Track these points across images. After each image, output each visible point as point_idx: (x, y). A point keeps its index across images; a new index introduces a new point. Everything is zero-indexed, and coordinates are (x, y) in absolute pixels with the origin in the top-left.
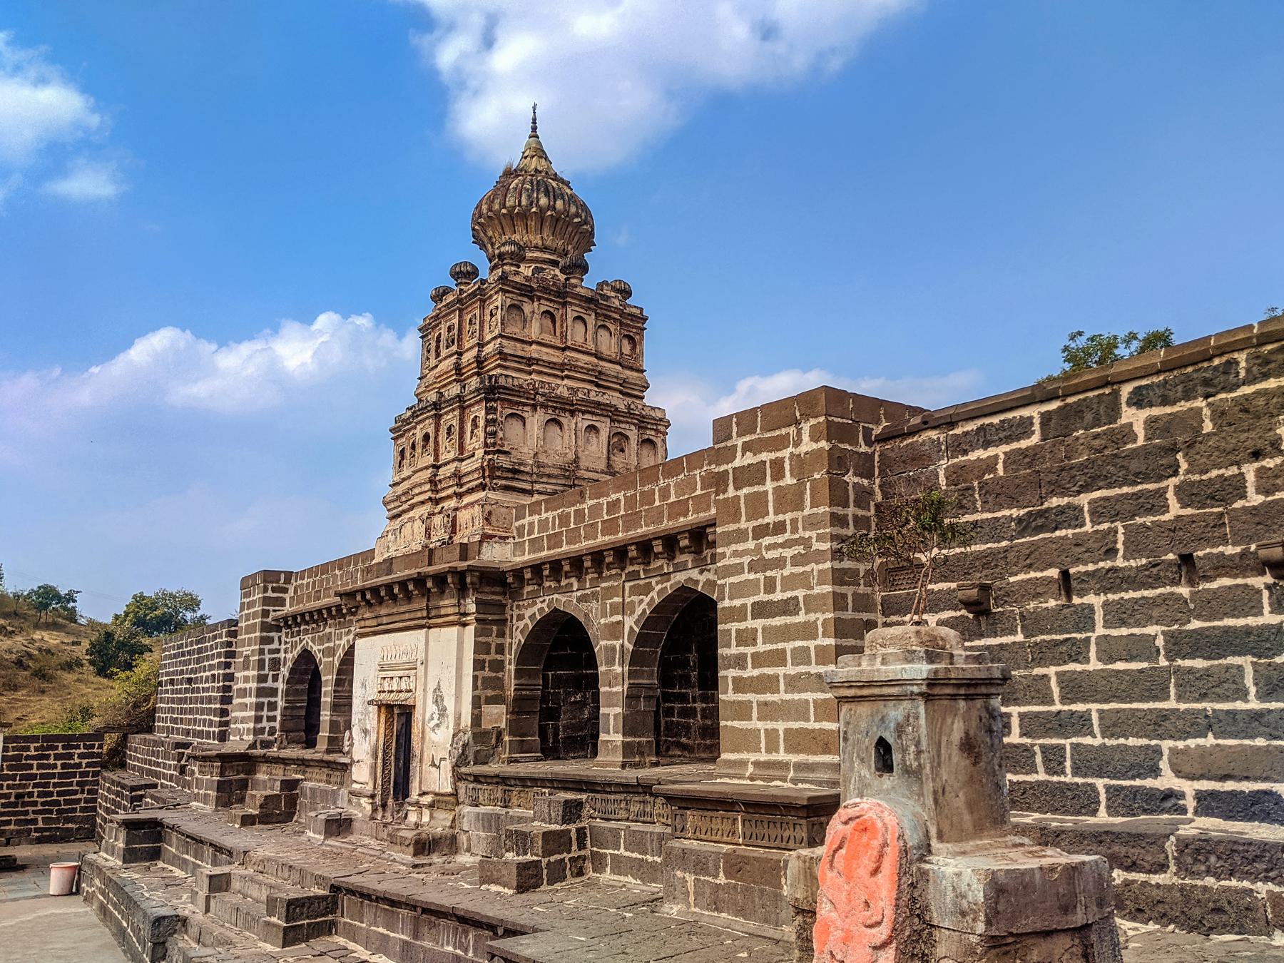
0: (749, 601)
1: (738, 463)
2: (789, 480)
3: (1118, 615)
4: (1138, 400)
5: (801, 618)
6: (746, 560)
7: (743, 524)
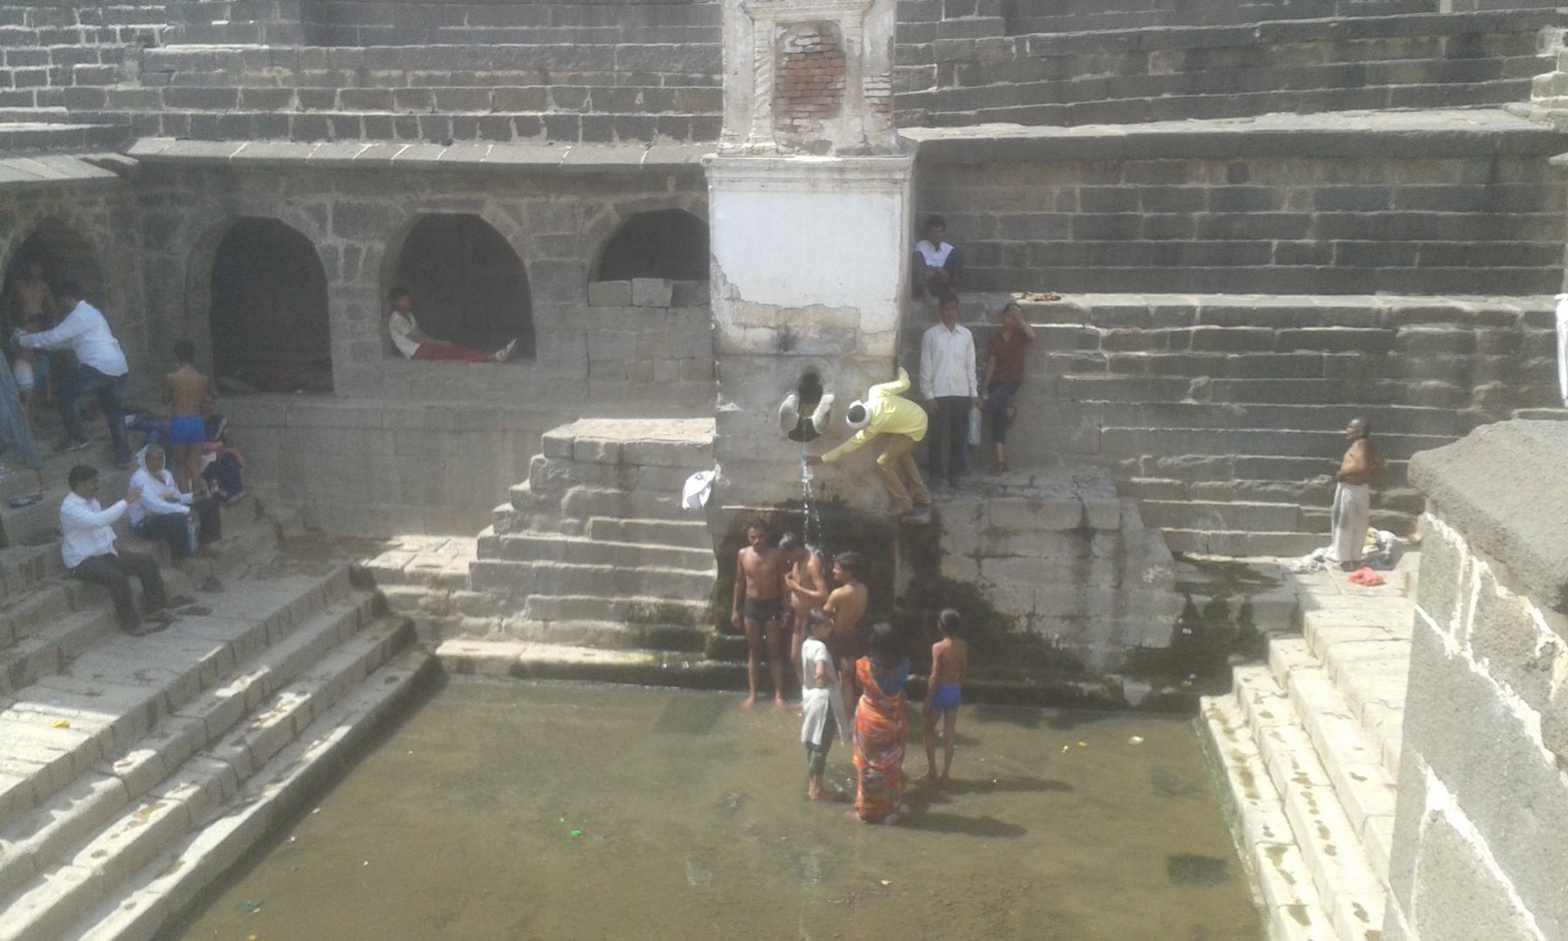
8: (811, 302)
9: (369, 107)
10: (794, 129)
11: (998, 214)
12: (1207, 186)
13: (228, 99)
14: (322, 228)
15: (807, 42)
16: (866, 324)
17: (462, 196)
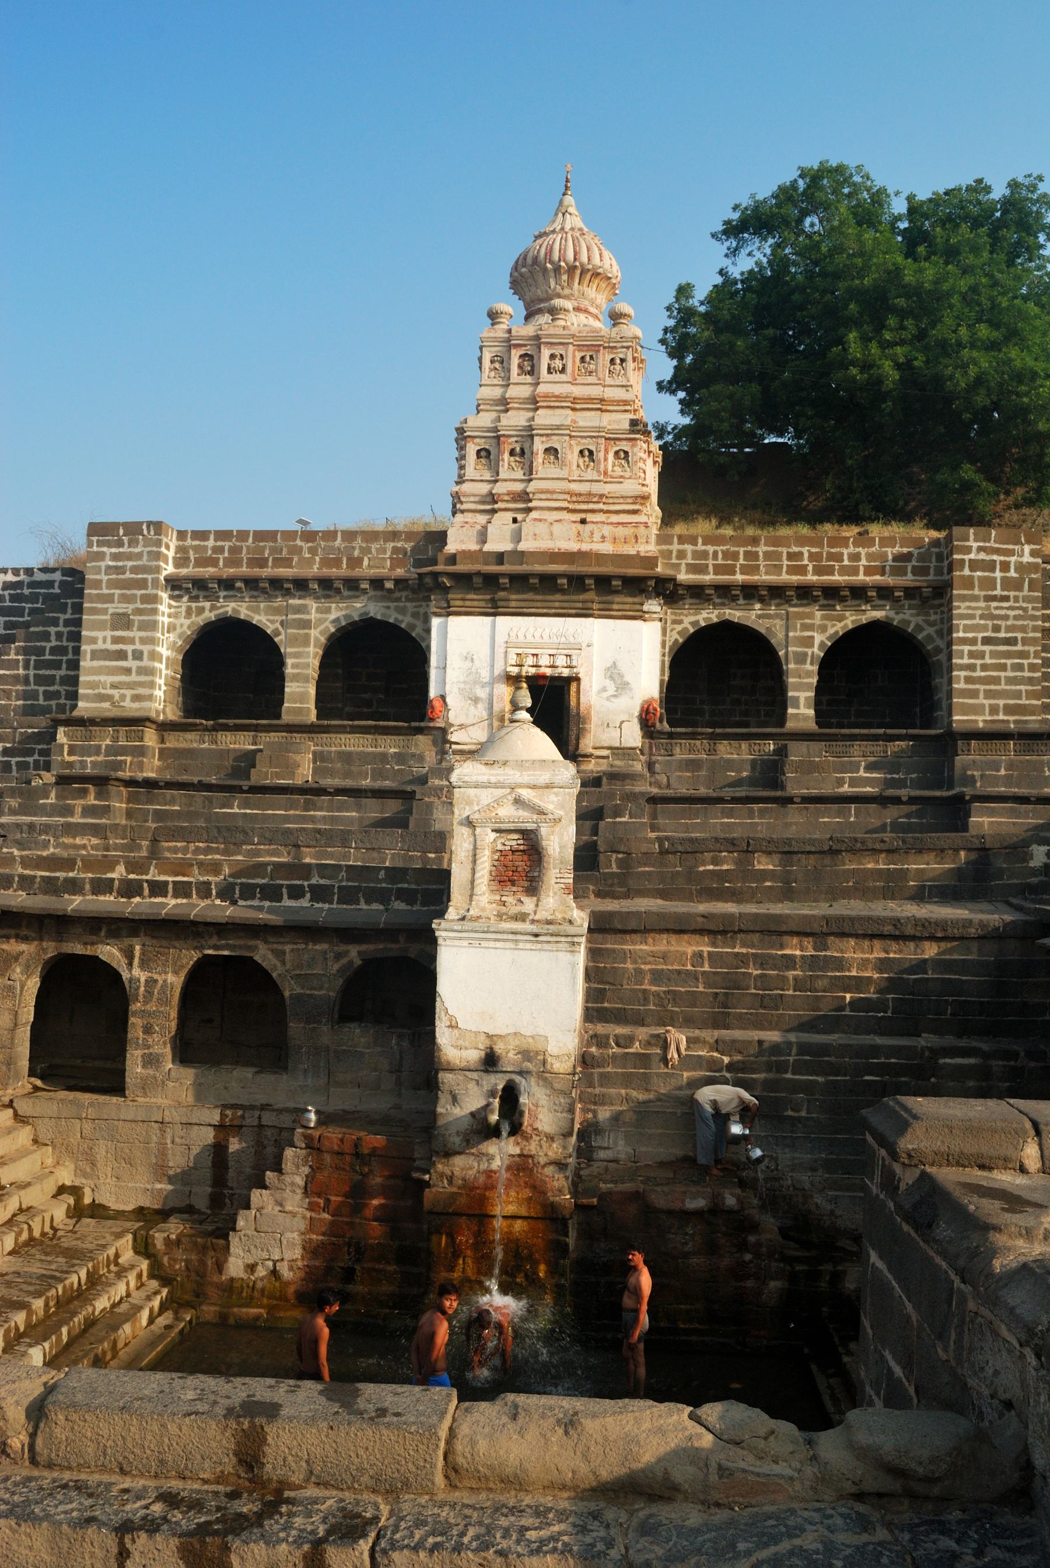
0: (980, 635)
1: (972, 556)
2: (1012, 573)
5: (1019, 647)
6: (980, 612)
7: (976, 592)
8: (511, 1030)
9: (177, 875)
10: (504, 904)
11: (648, 967)
12: (798, 953)
13: (68, 864)
14: (130, 964)
15: (514, 843)
16: (552, 1049)
17: (241, 942)
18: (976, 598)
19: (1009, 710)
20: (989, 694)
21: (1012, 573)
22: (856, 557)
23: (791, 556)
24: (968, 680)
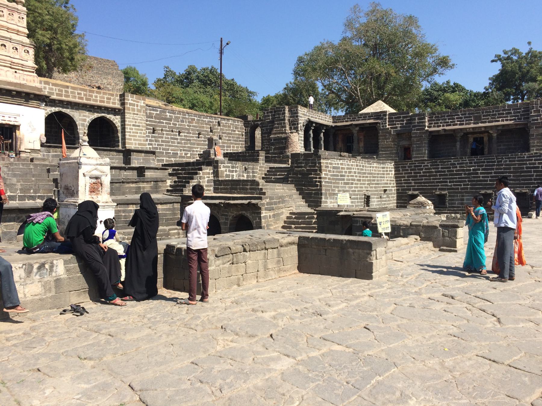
2: (139, 108)
3: (167, 134)
4: (168, 112)
5: (141, 128)
18: (130, 113)
19: (139, 144)
20: (134, 140)
21: (139, 108)
22: (96, 97)
23: (78, 94)
24: (130, 136)
